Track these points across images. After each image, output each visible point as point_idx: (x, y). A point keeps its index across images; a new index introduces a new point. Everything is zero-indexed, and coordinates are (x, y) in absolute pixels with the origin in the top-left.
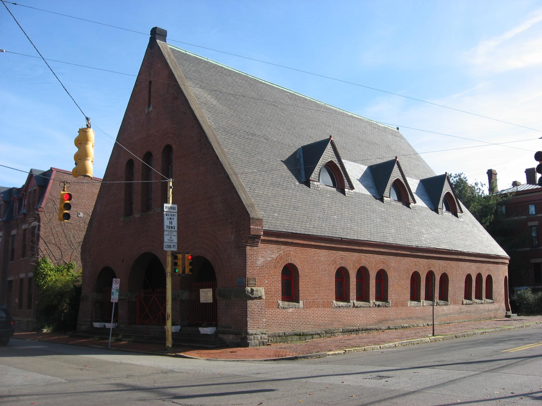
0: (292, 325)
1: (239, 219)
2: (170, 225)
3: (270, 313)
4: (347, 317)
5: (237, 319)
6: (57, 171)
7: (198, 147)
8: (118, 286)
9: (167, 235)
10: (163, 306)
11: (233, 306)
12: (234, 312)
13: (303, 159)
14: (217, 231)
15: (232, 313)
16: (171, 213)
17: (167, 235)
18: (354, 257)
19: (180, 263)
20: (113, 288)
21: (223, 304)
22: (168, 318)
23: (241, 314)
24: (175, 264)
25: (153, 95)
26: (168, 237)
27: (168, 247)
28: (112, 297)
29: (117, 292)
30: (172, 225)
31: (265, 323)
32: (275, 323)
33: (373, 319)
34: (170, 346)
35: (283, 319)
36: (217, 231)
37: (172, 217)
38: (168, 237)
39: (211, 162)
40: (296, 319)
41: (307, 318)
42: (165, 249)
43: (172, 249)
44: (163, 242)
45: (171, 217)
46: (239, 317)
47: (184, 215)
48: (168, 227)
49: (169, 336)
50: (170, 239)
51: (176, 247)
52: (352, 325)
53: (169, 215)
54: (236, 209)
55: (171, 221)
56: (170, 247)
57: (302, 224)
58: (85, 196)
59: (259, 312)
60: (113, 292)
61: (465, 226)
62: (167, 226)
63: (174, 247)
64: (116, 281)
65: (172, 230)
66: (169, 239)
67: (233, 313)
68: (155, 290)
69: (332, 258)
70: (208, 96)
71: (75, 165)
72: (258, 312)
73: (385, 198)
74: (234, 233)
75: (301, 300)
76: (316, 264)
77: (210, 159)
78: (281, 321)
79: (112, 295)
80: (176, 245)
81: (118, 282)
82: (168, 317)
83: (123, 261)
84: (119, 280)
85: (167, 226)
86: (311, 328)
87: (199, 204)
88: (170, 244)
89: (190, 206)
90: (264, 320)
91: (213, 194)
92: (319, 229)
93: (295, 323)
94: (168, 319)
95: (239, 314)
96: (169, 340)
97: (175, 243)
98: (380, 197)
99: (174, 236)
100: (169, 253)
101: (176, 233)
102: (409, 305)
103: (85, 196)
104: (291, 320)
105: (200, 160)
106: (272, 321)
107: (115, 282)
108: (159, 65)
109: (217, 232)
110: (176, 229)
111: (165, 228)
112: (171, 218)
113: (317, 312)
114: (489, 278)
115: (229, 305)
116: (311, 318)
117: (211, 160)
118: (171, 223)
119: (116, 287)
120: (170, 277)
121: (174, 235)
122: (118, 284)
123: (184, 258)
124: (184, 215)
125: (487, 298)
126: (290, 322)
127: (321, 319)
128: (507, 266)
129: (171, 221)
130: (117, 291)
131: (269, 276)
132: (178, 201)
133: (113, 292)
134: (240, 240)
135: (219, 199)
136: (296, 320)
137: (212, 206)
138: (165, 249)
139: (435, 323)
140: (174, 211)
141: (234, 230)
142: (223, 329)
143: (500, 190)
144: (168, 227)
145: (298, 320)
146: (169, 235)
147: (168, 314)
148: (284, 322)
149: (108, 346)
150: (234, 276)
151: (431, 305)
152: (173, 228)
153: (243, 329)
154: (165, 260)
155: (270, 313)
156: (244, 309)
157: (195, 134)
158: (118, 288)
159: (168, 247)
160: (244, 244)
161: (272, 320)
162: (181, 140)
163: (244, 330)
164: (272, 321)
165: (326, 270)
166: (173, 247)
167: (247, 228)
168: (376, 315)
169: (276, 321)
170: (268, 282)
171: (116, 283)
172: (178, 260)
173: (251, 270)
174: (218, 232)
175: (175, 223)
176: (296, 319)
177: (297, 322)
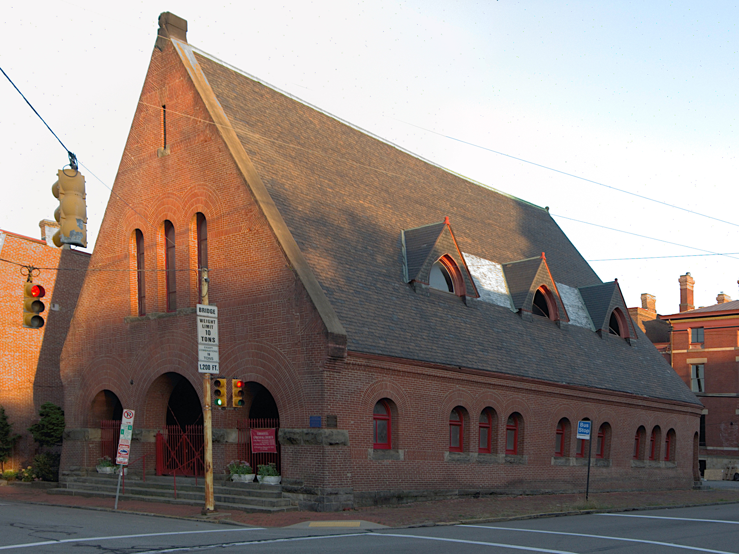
0: (389, 483)
1: (313, 333)
2: (208, 336)
3: (357, 465)
4: (465, 475)
5: (310, 472)
6: (7, 235)
7: (247, 221)
8: (131, 420)
9: (204, 350)
10: (198, 450)
11: (305, 454)
12: (305, 463)
13: (405, 248)
14: (279, 347)
15: (303, 464)
16: (208, 319)
17: (204, 350)
18: (477, 393)
19: (224, 390)
20: (124, 424)
21: (289, 451)
22: (207, 469)
23: (316, 465)
24: (217, 393)
25: (170, 129)
26: (205, 354)
27: (205, 368)
28: (121, 436)
29: (129, 429)
30: (210, 337)
31: (349, 479)
32: (364, 479)
33: (502, 479)
34: (212, 508)
35: (375, 474)
36: (279, 347)
37: (209, 324)
38: (205, 354)
39: (267, 246)
40: (393, 474)
41: (409, 474)
42: (200, 371)
43: (211, 371)
44: (197, 360)
45: (208, 324)
46: (313, 470)
47: (228, 321)
48: (204, 339)
49: (210, 495)
50: (208, 356)
51: (217, 368)
52: (472, 486)
53: (206, 322)
54: (307, 319)
55: (208, 329)
56: (208, 368)
57: (404, 344)
58: (62, 278)
59: (342, 463)
60: (123, 430)
61: (641, 358)
62: (203, 337)
63: (214, 369)
64: (128, 413)
65: (210, 343)
66: (207, 356)
67: (304, 463)
68: (186, 427)
69: (446, 393)
70: (261, 141)
71: (39, 227)
72: (340, 463)
73: (524, 312)
74: (305, 353)
75: (401, 449)
76: (423, 400)
77: (266, 241)
78: (373, 476)
79: (122, 434)
80: (217, 365)
81: (131, 416)
82: (208, 468)
83: (132, 383)
84: (133, 412)
85: (203, 337)
86: (415, 487)
87: (251, 306)
88: (208, 364)
89: (237, 308)
90: (349, 475)
91: (272, 294)
92: (428, 353)
93: (392, 479)
94: (207, 471)
95: (313, 465)
96: (209, 500)
97: (216, 362)
98: (518, 310)
99: (215, 353)
100: (207, 377)
101: (216, 348)
102: (552, 463)
103: (62, 278)
104: (387, 475)
105: (251, 241)
106: (360, 476)
107: (126, 414)
108: (177, 81)
109: (279, 349)
110: (217, 342)
111: (200, 340)
112: (208, 326)
113: (423, 466)
114: (671, 432)
115: (299, 453)
116: (414, 474)
117: (268, 243)
118: (209, 333)
119: (127, 423)
120: (210, 411)
121: (215, 351)
122: (131, 417)
123: (229, 383)
124: (228, 321)
125: (667, 459)
126: (386, 478)
127: (429, 476)
128: (699, 418)
129: (208, 329)
130: (130, 428)
131: (356, 415)
132: (218, 300)
133: (123, 430)
134: (313, 362)
135: (282, 301)
136: (394, 476)
137: (271, 311)
138: (200, 371)
139: (590, 490)
140: (213, 315)
141: (305, 348)
142: (289, 485)
143: (696, 308)
144: (204, 339)
145: (397, 476)
146: (205, 350)
147: (208, 463)
148: (377, 478)
149: (114, 508)
150: (305, 413)
151: (585, 465)
152: (212, 340)
153: (318, 487)
154: (202, 385)
155: (357, 465)
156: (320, 459)
157: (241, 200)
158: (132, 424)
159: (205, 368)
160: (319, 369)
161: (360, 474)
162: (220, 208)
163: (319, 488)
164: (360, 476)
165: (437, 410)
166: (213, 368)
167: (323, 346)
168: (506, 474)
169: (365, 477)
170: (354, 422)
171: (129, 417)
172: (221, 387)
173: (330, 405)
174: (281, 349)
175: (215, 333)
176: (393, 474)
177: (396, 478)
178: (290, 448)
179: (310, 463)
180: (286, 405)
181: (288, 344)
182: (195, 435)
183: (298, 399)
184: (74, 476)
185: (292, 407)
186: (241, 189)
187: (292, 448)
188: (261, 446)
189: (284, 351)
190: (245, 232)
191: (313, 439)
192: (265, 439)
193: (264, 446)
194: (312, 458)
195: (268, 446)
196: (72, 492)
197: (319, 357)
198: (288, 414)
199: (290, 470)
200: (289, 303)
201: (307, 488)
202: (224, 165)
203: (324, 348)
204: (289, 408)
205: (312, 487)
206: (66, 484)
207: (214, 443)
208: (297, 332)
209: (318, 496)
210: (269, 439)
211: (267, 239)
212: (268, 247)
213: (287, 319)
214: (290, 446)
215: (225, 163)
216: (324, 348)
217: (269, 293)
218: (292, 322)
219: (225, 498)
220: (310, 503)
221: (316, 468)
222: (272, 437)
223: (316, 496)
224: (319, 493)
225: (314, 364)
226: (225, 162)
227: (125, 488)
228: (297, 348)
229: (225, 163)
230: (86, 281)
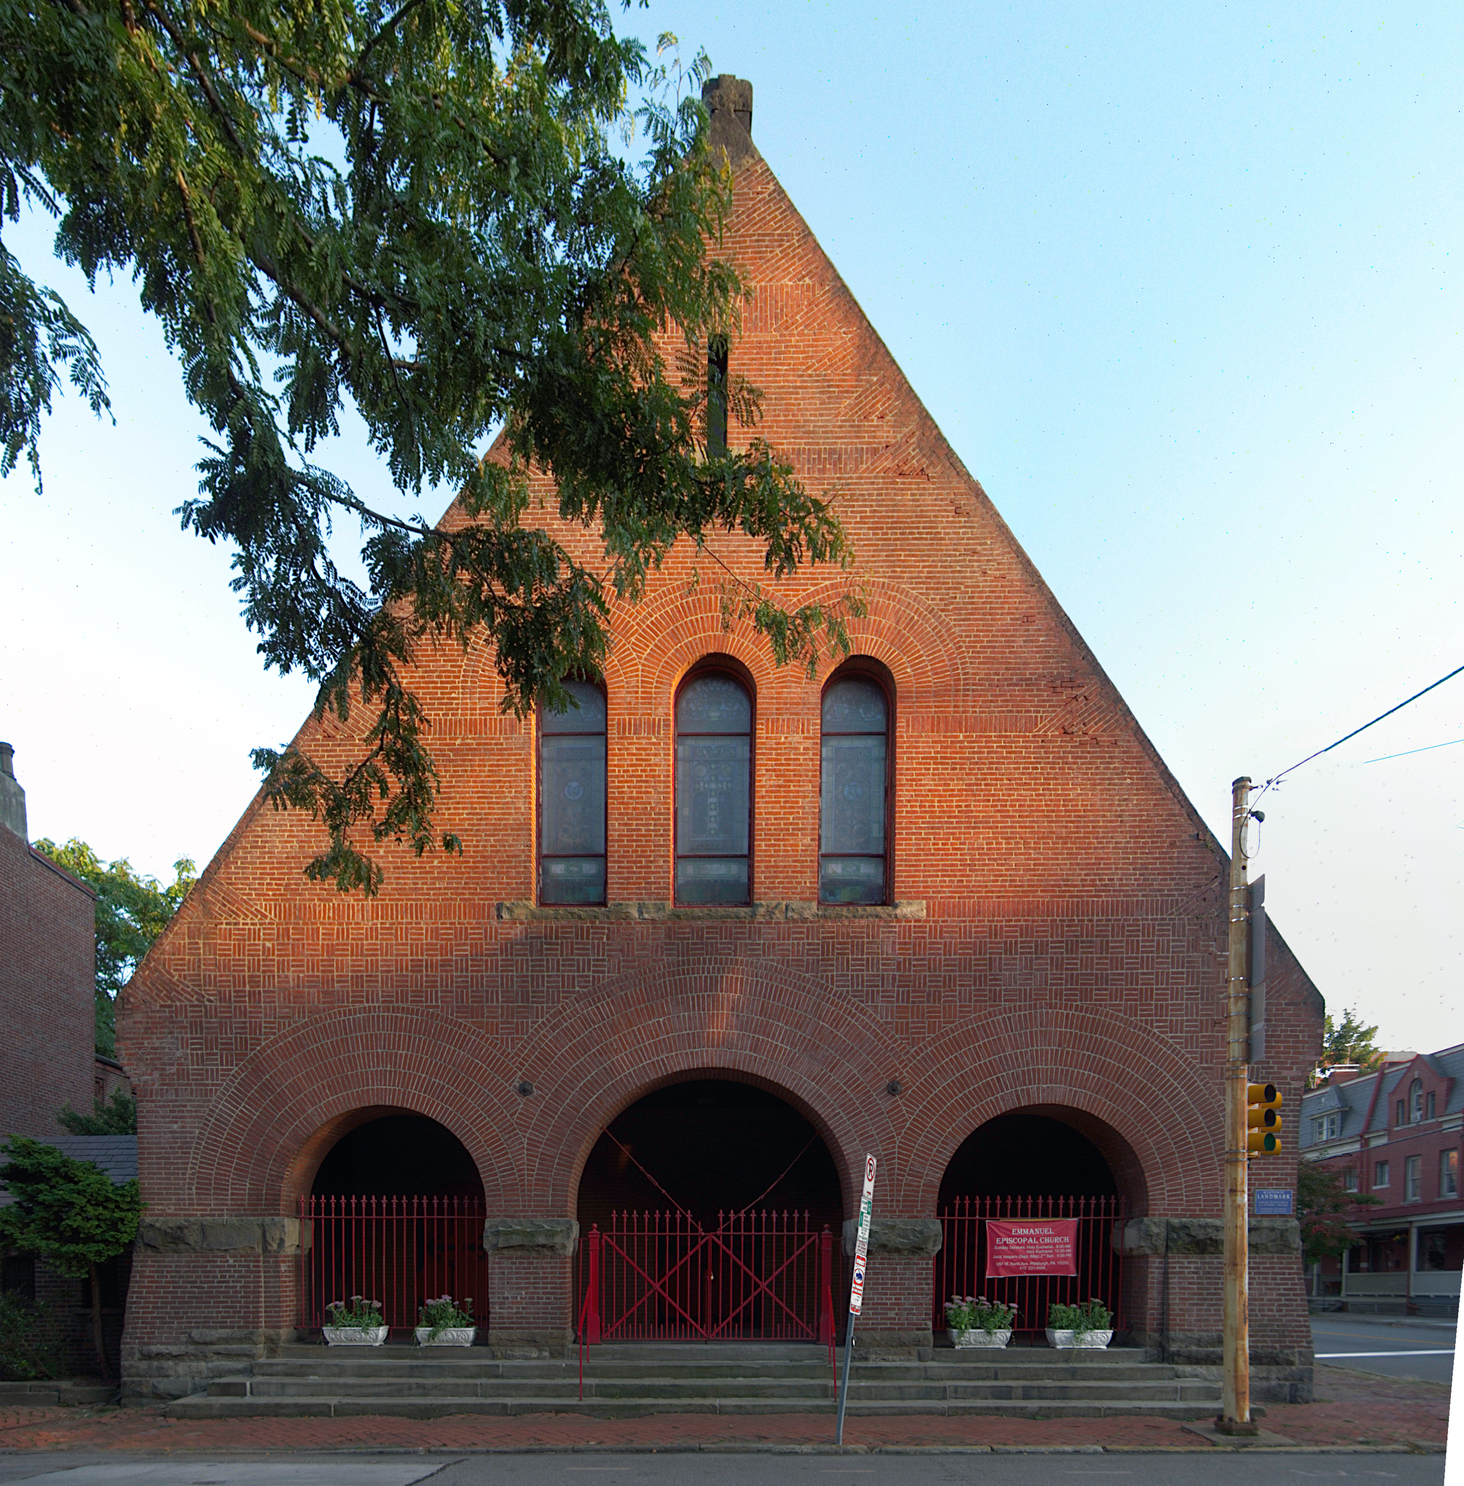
14: (1157, 1027)
36: (1157, 1027)
142: (1194, 1348)
160: (1289, 1084)
178: (1189, 1263)
179: (1260, 1294)
180: (1176, 1163)
181: (1187, 1021)
182: (780, 1238)
183: (1216, 1151)
184: (215, 1357)
185: (1196, 1169)
186: (1039, 624)
187: (1196, 1263)
188: (1023, 1260)
189: (1172, 1038)
190: (1049, 734)
191: (1274, 1241)
192: (1040, 1245)
193: (1034, 1260)
194: (1266, 1284)
195: (1049, 1260)
196: (329, 1406)
197: (1290, 1058)
198: (1180, 1184)
199: (1195, 1313)
200: (1196, 925)
201: (1259, 1351)
202: (975, 552)
203: (1309, 1037)
204: (1184, 1171)
205: (1275, 1348)
206: (244, 1385)
207: (1253, 1233)
208: (1221, 996)
209: (1294, 1368)
210: (1054, 1245)
211: (1126, 763)
212: (1132, 784)
213: (1188, 962)
214: (1187, 1258)
215: (979, 548)
216: (1309, 1037)
217: (1129, 896)
218: (1206, 969)
219: (956, 1388)
220: (1265, 1384)
221: (1279, 1305)
222: (1066, 1239)
223: (1287, 1367)
224: (1296, 1359)
225: (1275, 1073)
226: (980, 544)
227: (585, 1381)
228: (1218, 1032)
229: (979, 548)
230: (724, 688)
